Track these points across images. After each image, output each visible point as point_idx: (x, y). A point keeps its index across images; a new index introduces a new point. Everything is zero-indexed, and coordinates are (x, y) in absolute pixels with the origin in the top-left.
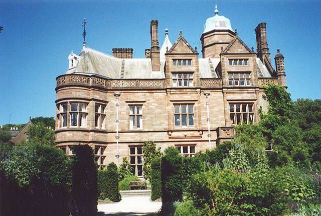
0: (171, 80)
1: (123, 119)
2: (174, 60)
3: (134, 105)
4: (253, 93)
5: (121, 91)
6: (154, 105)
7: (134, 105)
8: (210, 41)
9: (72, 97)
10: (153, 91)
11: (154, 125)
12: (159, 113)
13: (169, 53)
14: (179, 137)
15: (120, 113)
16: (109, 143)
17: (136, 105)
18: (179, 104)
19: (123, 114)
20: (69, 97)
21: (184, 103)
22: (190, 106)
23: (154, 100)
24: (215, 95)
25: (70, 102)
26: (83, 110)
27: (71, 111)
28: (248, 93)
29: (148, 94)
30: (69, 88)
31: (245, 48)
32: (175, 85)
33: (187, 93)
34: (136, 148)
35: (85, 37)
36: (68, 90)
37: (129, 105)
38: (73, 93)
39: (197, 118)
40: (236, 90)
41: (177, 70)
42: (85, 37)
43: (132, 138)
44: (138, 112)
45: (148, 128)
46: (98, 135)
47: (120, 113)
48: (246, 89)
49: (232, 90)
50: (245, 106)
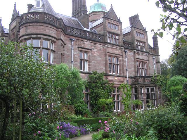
1: (76, 62)
6: (96, 54)
8: (98, 17)
9: (46, 34)
10: (96, 43)
11: (109, 75)
12: (100, 61)
16: (15, 8)
20: (44, 33)
23: (97, 50)
24: (129, 53)
30: (43, 24)
35: (15, 6)
36: (42, 27)
38: (47, 30)
39: (122, 68)
41: (111, 31)
42: (15, 6)
46: (32, 31)
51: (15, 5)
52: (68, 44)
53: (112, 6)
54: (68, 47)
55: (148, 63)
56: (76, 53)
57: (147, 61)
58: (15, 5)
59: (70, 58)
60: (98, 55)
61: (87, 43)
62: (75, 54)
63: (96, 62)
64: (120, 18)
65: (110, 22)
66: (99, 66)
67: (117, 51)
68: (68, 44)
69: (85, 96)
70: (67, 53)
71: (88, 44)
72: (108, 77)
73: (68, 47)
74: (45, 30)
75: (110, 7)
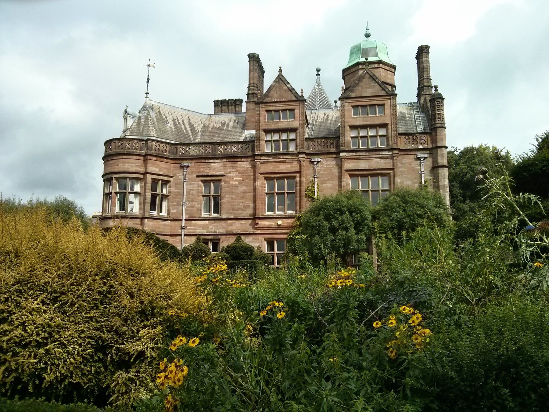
0: (262, 143)
2: (268, 111)
3: (207, 180)
4: (387, 158)
5: (190, 161)
7: (207, 180)
10: (236, 160)
13: (260, 101)
14: (269, 228)
15: (188, 193)
17: (212, 181)
18: (273, 179)
19: (192, 195)
21: (281, 177)
22: (363, 178)
25: (117, 179)
26: (165, 192)
27: (117, 190)
28: (381, 158)
29: (229, 165)
31: (378, 87)
32: (267, 150)
33: (284, 161)
34: (275, 242)
35: (148, 85)
37: (202, 181)
38: (120, 165)
40: (361, 154)
41: (273, 127)
42: (148, 85)
43: (203, 229)
44: (162, 192)
45: (227, 213)
47: (188, 193)
48: (377, 153)
49: (354, 154)
50: (157, 183)
51: (148, 79)
52: (178, 175)
53: (280, 71)
54: (178, 179)
55: (392, 174)
56: (193, 187)
57: (392, 171)
58: (148, 79)
59: (181, 197)
60: (239, 182)
61: (216, 164)
62: (192, 188)
63: (234, 196)
64: (302, 90)
65: (271, 109)
66: (241, 202)
67: (289, 166)
68: (178, 175)
69: (151, 223)
70: (176, 190)
71: (219, 166)
72: (257, 221)
73: (178, 179)
74: (118, 165)
75: (278, 73)
